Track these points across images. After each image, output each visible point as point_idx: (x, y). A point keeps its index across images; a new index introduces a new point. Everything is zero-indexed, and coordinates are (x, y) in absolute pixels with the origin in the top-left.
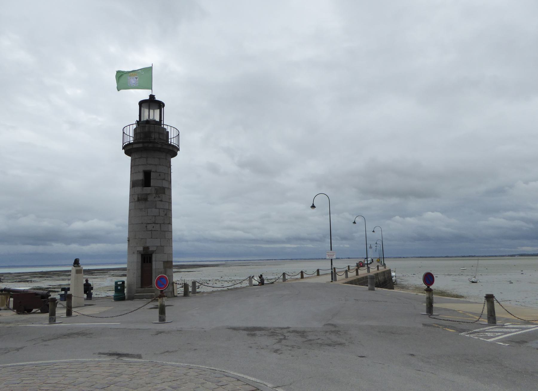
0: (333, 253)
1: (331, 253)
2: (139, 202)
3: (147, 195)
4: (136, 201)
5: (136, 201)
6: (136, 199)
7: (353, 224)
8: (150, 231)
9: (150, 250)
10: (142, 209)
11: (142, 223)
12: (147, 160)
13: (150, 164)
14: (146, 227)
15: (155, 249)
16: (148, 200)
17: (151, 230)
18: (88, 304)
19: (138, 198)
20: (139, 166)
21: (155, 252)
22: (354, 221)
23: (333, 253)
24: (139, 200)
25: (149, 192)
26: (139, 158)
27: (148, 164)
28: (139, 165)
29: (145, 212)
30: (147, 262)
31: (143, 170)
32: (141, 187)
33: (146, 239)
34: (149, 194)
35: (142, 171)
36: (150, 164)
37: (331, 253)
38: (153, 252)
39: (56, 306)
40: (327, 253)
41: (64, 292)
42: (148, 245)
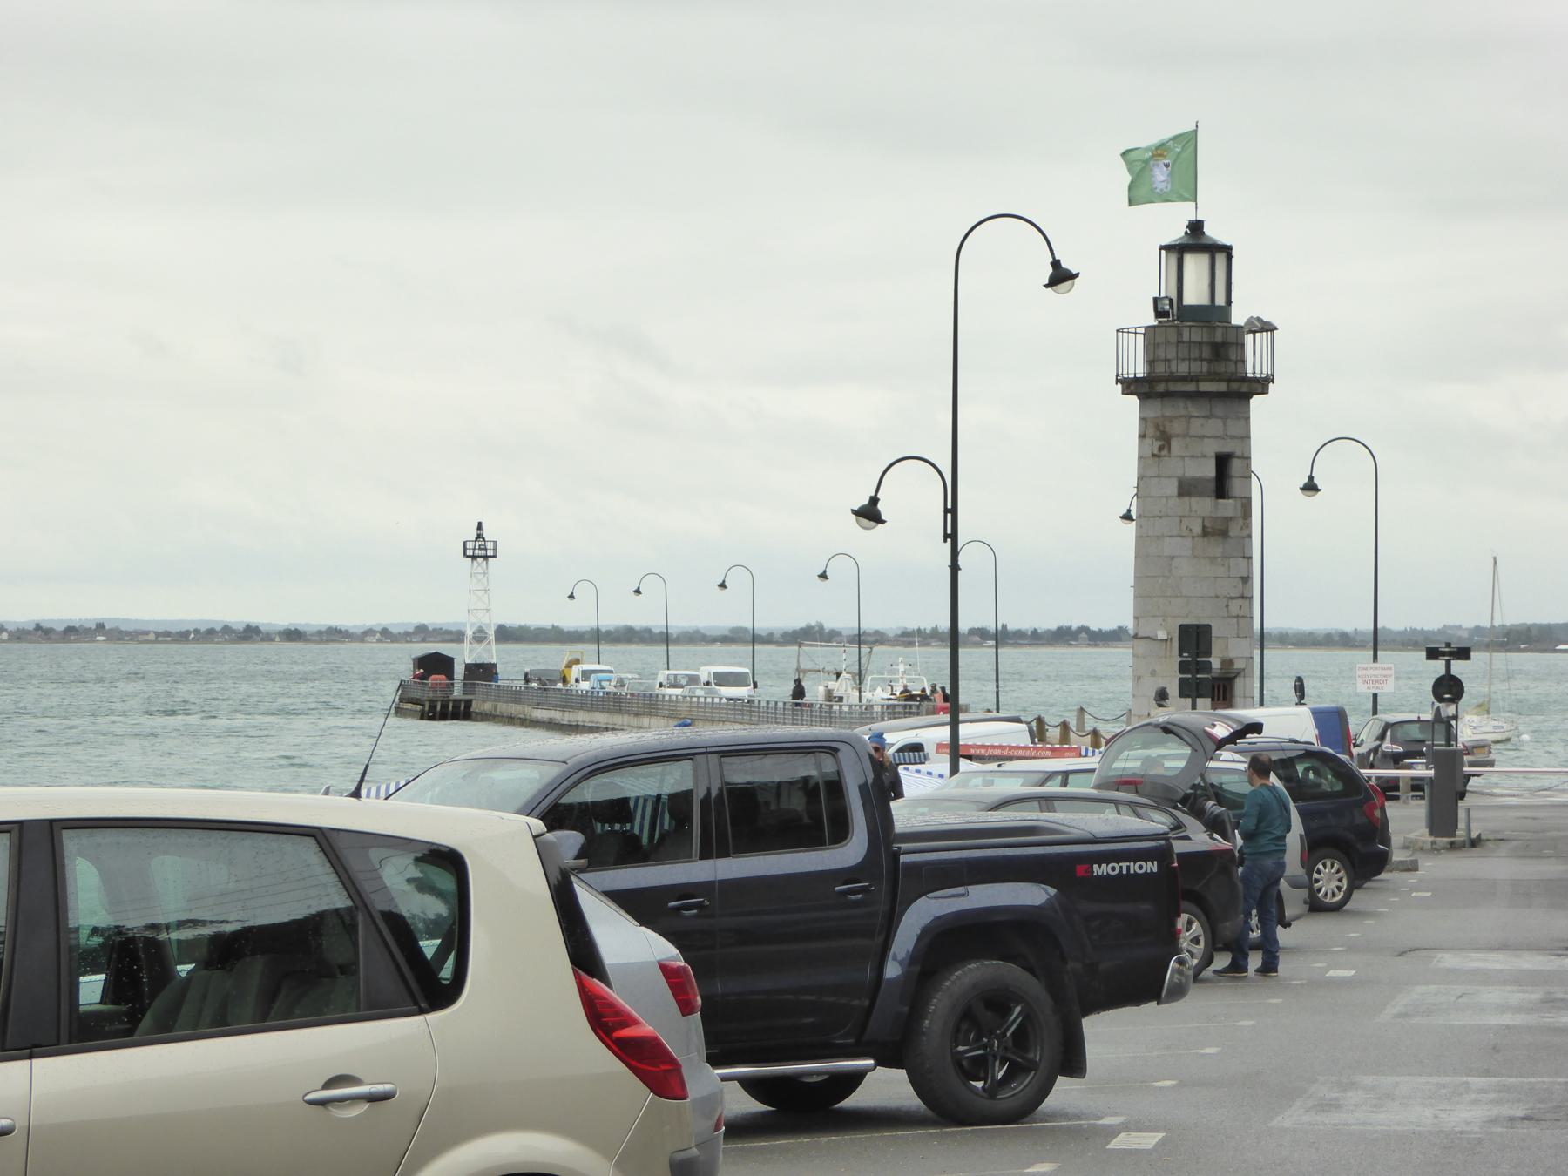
0: (1384, 672)
1: (1376, 672)
2: (1206, 540)
3: (1228, 520)
4: (1198, 536)
5: (1198, 536)
6: (1197, 529)
7: (819, 581)
8: (1235, 617)
9: (1235, 667)
10: (1215, 558)
11: (1217, 597)
12: (1224, 424)
13: (1233, 437)
14: (1227, 606)
15: (1243, 666)
16: (1231, 534)
17: (1237, 617)
18: (1040, 760)
19: (1204, 527)
20: (1206, 440)
21: (1242, 674)
22: (822, 572)
23: (1384, 672)
24: (1205, 533)
25: (1230, 514)
26: (1203, 417)
27: (1227, 436)
28: (1204, 437)
29: (1223, 565)
30: (1218, 700)
31: (1216, 453)
32: (1213, 498)
33: (1227, 638)
34: (1231, 518)
35: (1213, 454)
36: (1233, 437)
37: (1376, 672)
38: (1238, 674)
39: (1457, 828)
40: (1359, 673)
41: (422, 670)
42: (1232, 654)
